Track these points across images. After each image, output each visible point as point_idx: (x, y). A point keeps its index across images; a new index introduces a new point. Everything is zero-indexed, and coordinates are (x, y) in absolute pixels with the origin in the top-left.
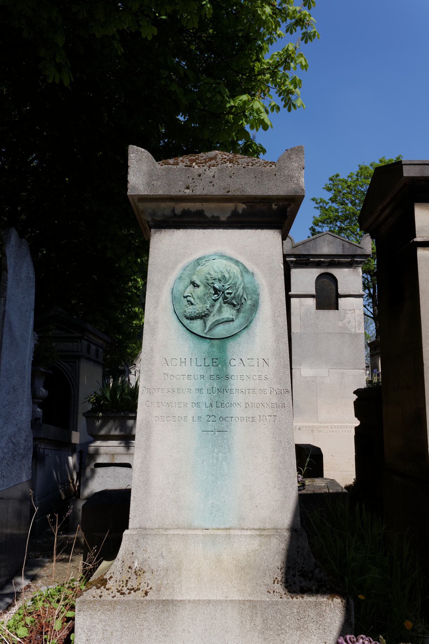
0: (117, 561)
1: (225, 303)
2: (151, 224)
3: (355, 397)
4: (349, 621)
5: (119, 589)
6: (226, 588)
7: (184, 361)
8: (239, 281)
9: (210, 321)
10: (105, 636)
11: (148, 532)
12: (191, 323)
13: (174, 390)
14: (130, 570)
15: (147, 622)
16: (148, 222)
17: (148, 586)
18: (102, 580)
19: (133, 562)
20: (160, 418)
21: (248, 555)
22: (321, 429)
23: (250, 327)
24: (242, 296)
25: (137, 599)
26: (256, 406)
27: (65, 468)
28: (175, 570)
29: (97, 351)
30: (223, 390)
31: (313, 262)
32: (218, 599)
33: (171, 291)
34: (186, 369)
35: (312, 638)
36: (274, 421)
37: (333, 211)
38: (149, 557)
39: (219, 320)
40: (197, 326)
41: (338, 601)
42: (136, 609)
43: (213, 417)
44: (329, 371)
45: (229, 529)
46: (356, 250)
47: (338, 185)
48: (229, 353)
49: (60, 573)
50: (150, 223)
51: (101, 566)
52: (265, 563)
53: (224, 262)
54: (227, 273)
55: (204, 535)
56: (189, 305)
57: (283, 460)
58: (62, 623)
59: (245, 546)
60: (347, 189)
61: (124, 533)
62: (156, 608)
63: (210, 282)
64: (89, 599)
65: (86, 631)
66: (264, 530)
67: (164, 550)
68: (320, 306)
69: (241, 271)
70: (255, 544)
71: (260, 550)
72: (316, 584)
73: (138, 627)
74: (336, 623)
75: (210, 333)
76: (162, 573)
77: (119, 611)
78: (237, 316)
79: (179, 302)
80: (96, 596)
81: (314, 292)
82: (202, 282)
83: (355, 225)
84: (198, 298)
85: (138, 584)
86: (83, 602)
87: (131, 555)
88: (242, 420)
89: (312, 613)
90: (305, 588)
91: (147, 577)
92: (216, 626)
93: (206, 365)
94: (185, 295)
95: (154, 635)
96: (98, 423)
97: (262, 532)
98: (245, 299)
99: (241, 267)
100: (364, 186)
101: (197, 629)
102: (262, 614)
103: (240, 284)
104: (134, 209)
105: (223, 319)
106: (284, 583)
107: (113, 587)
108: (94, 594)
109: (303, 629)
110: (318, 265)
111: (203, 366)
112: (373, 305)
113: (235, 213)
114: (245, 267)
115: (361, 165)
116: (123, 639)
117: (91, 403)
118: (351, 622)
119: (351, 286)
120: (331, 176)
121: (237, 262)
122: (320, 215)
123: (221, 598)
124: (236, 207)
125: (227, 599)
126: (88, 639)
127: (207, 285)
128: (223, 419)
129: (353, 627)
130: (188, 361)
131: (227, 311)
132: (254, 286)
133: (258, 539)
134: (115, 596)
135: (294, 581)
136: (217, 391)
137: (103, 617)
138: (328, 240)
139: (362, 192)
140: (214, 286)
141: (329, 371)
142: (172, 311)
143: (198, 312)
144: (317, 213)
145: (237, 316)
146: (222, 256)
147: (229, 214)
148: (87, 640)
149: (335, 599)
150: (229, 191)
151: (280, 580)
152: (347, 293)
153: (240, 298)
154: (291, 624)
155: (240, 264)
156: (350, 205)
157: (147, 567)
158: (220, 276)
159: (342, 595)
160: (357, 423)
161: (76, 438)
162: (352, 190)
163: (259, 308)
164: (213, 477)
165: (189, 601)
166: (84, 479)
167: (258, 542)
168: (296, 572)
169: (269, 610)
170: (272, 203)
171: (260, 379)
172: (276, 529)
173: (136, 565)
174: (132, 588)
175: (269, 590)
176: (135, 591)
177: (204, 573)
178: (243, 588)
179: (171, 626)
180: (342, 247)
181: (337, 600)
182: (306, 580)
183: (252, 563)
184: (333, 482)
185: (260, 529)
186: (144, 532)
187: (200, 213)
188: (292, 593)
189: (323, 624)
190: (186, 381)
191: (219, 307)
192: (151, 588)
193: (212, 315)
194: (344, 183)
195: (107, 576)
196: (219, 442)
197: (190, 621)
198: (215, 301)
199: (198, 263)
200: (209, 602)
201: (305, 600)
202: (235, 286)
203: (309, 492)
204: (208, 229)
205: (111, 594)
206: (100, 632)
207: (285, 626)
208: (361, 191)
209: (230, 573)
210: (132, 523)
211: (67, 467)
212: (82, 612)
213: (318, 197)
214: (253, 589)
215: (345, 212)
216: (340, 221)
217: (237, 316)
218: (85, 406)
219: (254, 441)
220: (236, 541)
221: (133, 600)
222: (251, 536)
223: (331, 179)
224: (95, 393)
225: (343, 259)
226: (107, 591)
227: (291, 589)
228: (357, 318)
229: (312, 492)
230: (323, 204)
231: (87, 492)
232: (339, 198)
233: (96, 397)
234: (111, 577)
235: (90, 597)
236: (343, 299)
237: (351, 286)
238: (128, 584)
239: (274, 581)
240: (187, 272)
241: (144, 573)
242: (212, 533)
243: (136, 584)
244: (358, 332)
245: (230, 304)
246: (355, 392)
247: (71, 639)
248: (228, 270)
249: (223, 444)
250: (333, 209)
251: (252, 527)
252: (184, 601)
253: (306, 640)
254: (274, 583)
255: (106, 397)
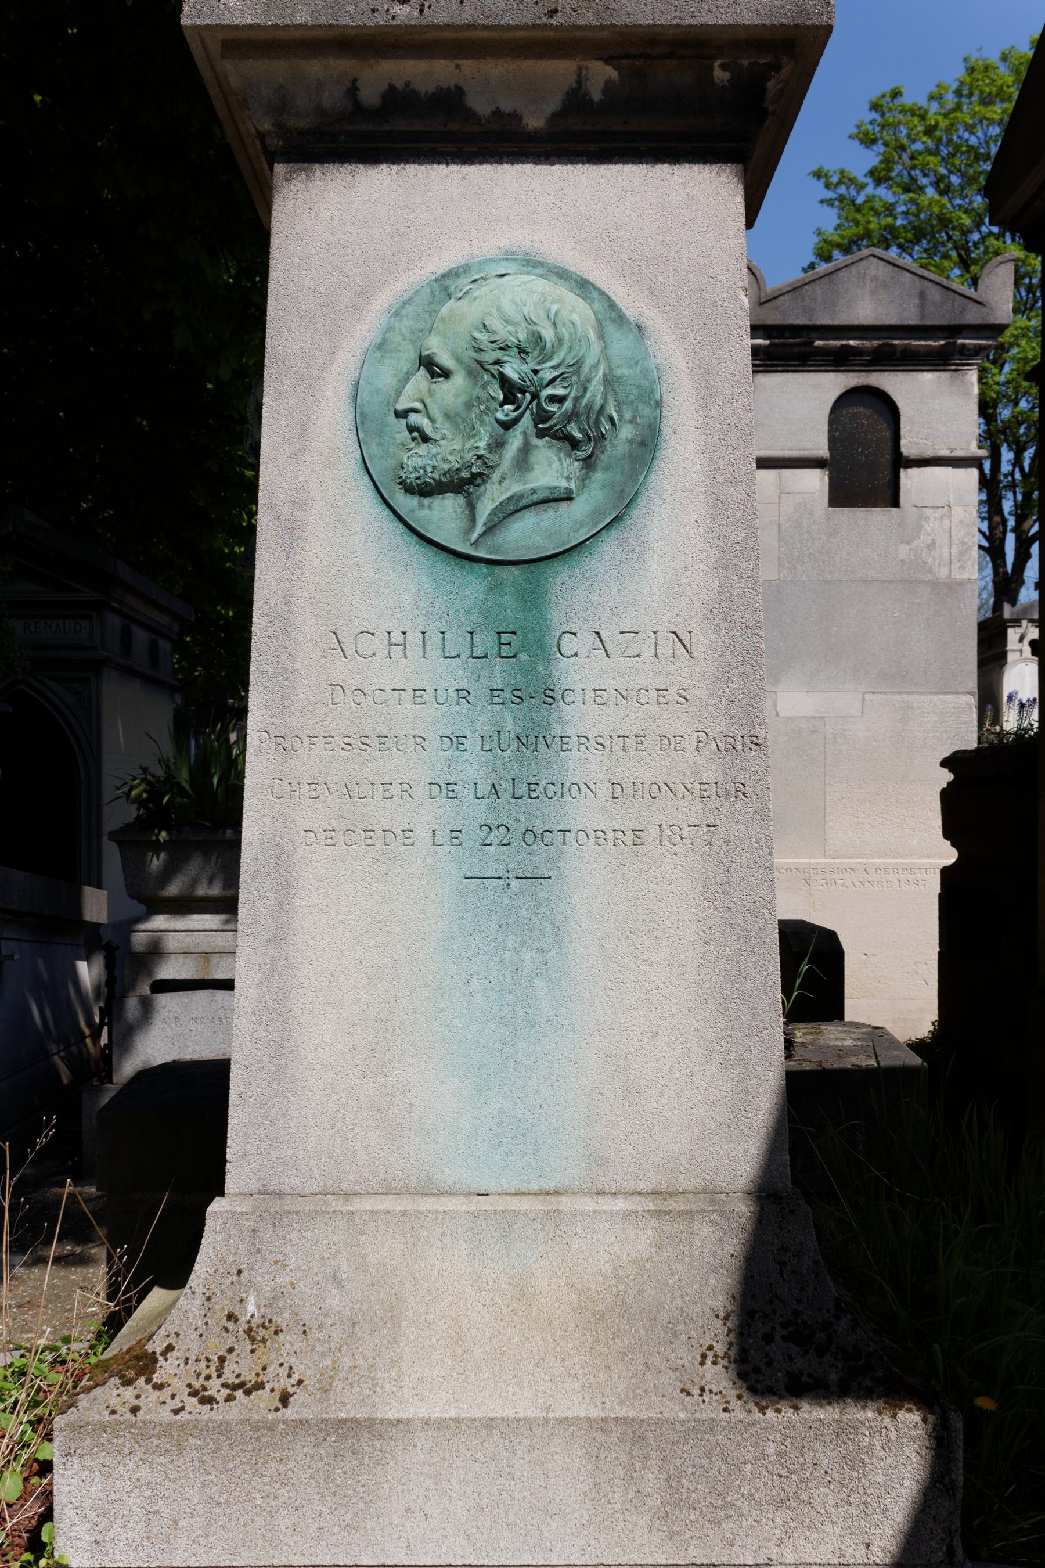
0: (190, 1296)
1: (541, 434)
2: (274, 143)
3: (946, 777)
4: (947, 1478)
5: (197, 1385)
6: (547, 1378)
7: (400, 639)
8: (592, 354)
9: (488, 503)
10: (154, 1530)
11: (289, 1204)
12: (421, 506)
13: (366, 740)
14: (230, 1325)
15: (290, 1487)
16: (261, 136)
17: (289, 1376)
18: (138, 1358)
19: (242, 1300)
20: (321, 835)
21: (616, 1276)
22: (836, 876)
23: (629, 522)
24: (602, 408)
25: (255, 1416)
26: (647, 791)
27: (68, 993)
28: (381, 1324)
29: (154, 646)
30: (534, 739)
31: (824, 351)
32: (521, 1415)
33: (349, 392)
34: (409, 669)
35: (824, 1531)
36: (710, 843)
37: (878, 214)
38: (292, 1284)
39: (520, 497)
40: (443, 516)
41: (910, 1418)
42: (250, 1448)
43: (502, 829)
44: (863, 699)
45: (557, 1193)
46: (963, 311)
47: (895, 126)
48: (555, 612)
49: (57, 1296)
50: (268, 141)
51: (145, 1304)
52: (673, 1299)
53: (540, 285)
54: (547, 324)
55: (475, 1215)
56: (413, 444)
57: (736, 971)
58: (26, 1479)
59: (610, 1245)
60: (924, 139)
61: (209, 1209)
62: (318, 1445)
63: (489, 356)
64: (97, 1417)
65: (92, 1515)
66: (672, 1194)
67: (342, 1260)
68: (842, 496)
69: (598, 320)
70: (641, 1241)
71: (656, 1259)
72: (840, 1365)
73: (259, 1501)
74: (902, 1485)
75: (489, 541)
76: (337, 1335)
77: (195, 1454)
78: (584, 480)
79: (380, 434)
80: (120, 1409)
81: (822, 450)
82: (459, 360)
83: (946, 256)
84: (447, 416)
85: (259, 1368)
86: (77, 1428)
87: (235, 1278)
88: (601, 841)
89: (827, 1457)
90: (805, 1379)
91: (287, 1346)
92: (512, 1499)
93: (478, 653)
94: (400, 407)
95: (314, 1527)
96: (156, 863)
97: (664, 1203)
98: (611, 419)
99: (597, 305)
100: (979, 127)
101: (451, 1508)
102: (664, 1459)
103: (595, 366)
104: (213, 91)
105: (534, 491)
106: (735, 1361)
107: (176, 1380)
108: (113, 1402)
109: (795, 1505)
110: (839, 361)
111: (464, 656)
112: (989, 512)
113: (576, 101)
114: (612, 306)
115: (973, 60)
116: (211, 1539)
117: (133, 802)
118: (952, 1482)
119: (943, 429)
120: (874, 95)
121: (584, 287)
122: (838, 227)
123: (530, 1414)
124: (579, 76)
125: (551, 1415)
126: (100, 1538)
127: (477, 369)
128: (533, 836)
129: (959, 1496)
130: (414, 639)
131: (550, 465)
132: (646, 372)
133: (652, 1224)
134: (183, 1408)
135: (767, 1355)
136: (515, 743)
137: (144, 1473)
138: (875, 278)
139: (971, 148)
140: (501, 374)
141: (863, 699)
142: (355, 465)
143: (446, 467)
144: (829, 220)
145: (583, 480)
146: (531, 263)
147: (553, 104)
148: (97, 1542)
149: (901, 1414)
150: (556, 11)
151: (721, 1354)
152: (929, 453)
153: (593, 416)
154: (757, 1490)
155: (595, 294)
156: (931, 192)
157: (286, 1315)
158: (522, 336)
159: (924, 1401)
160: (949, 855)
161: (96, 906)
162: (940, 140)
163: (660, 453)
164: (503, 1029)
165: (426, 1422)
166: (121, 1024)
167: (650, 1233)
168: (773, 1328)
169: (686, 1448)
170: (713, 58)
171: (662, 700)
172: (709, 1192)
173: (251, 1307)
174: (237, 1382)
175: (688, 1386)
176: (248, 1393)
177: (473, 1331)
178: (602, 1378)
179: (367, 1498)
180: (917, 301)
181: (907, 1415)
182: (807, 1352)
183: (630, 1300)
184: (877, 1035)
185: (656, 1193)
186: (276, 1206)
187: (449, 100)
188: (763, 1394)
189: (861, 1489)
190: (408, 705)
191: (519, 450)
192: (300, 1382)
193: (496, 476)
194: (916, 120)
195: (157, 1346)
196: (524, 913)
197: (429, 1482)
198: (507, 426)
199: (446, 289)
200: (490, 1424)
201: (805, 1415)
202: (578, 372)
203: (807, 1067)
204: (481, 163)
205: (168, 1400)
206: (136, 1518)
207: (736, 1496)
208: (968, 146)
209: (559, 1333)
210: (238, 1174)
211: (72, 991)
212: (76, 1460)
213: (832, 166)
214: (633, 1381)
215: (917, 216)
216: (900, 246)
217: (583, 480)
218: (118, 814)
219: (640, 909)
220: (579, 1230)
221: (241, 1422)
222: (627, 1215)
223: (875, 107)
224: (145, 770)
225: (920, 339)
226: (157, 1393)
227: (758, 1381)
228: (958, 534)
229: (816, 1067)
230: (848, 188)
231: (129, 1067)
232: (898, 168)
233: (149, 783)
234: (170, 1348)
235: (99, 1413)
236: (914, 472)
237: (943, 429)
238: (226, 1371)
239: (704, 1356)
240: (406, 323)
241: (276, 1333)
242: (501, 1208)
243: (251, 1369)
244: (958, 576)
245: (559, 439)
246: (945, 763)
247: (45, 1538)
248: (553, 312)
249: (535, 920)
250: (878, 205)
251: (631, 1186)
252: (408, 1421)
253: (806, 1538)
254: (702, 1363)
255: (179, 784)
